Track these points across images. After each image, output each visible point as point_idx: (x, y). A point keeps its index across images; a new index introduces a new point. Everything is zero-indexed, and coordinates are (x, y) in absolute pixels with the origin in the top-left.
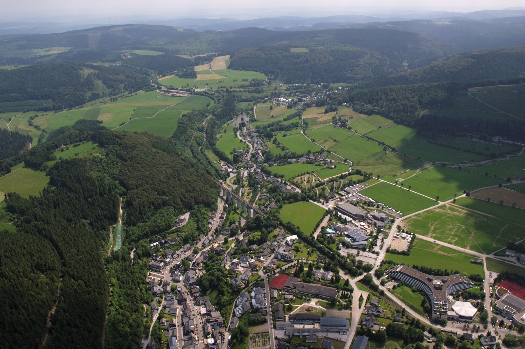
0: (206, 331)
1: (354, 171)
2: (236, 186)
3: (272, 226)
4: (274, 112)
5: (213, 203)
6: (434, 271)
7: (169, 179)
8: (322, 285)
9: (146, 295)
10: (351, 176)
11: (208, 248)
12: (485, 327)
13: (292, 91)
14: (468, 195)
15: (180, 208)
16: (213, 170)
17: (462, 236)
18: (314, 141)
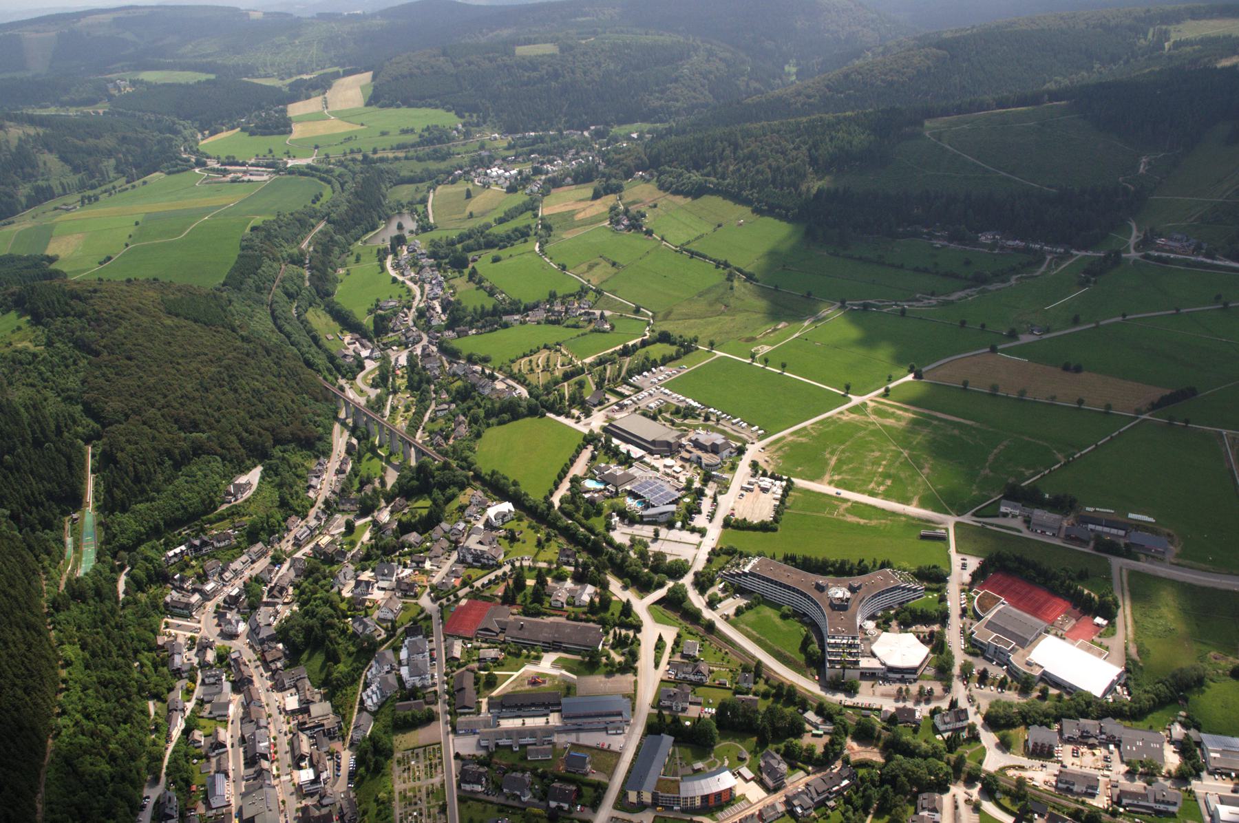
0: (297, 753)
1: (656, 334)
2: (379, 391)
3: (455, 484)
4: (474, 205)
5: (320, 439)
6: (833, 565)
7: (207, 390)
8: (568, 618)
9: (154, 678)
10: (648, 348)
11: (307, 549)
12: (947, 689)
13: (520, 150)
14: (918, 376)
15: (237, 457)
16: (323, 356)
17: (902, 475)
18: (564, 268)
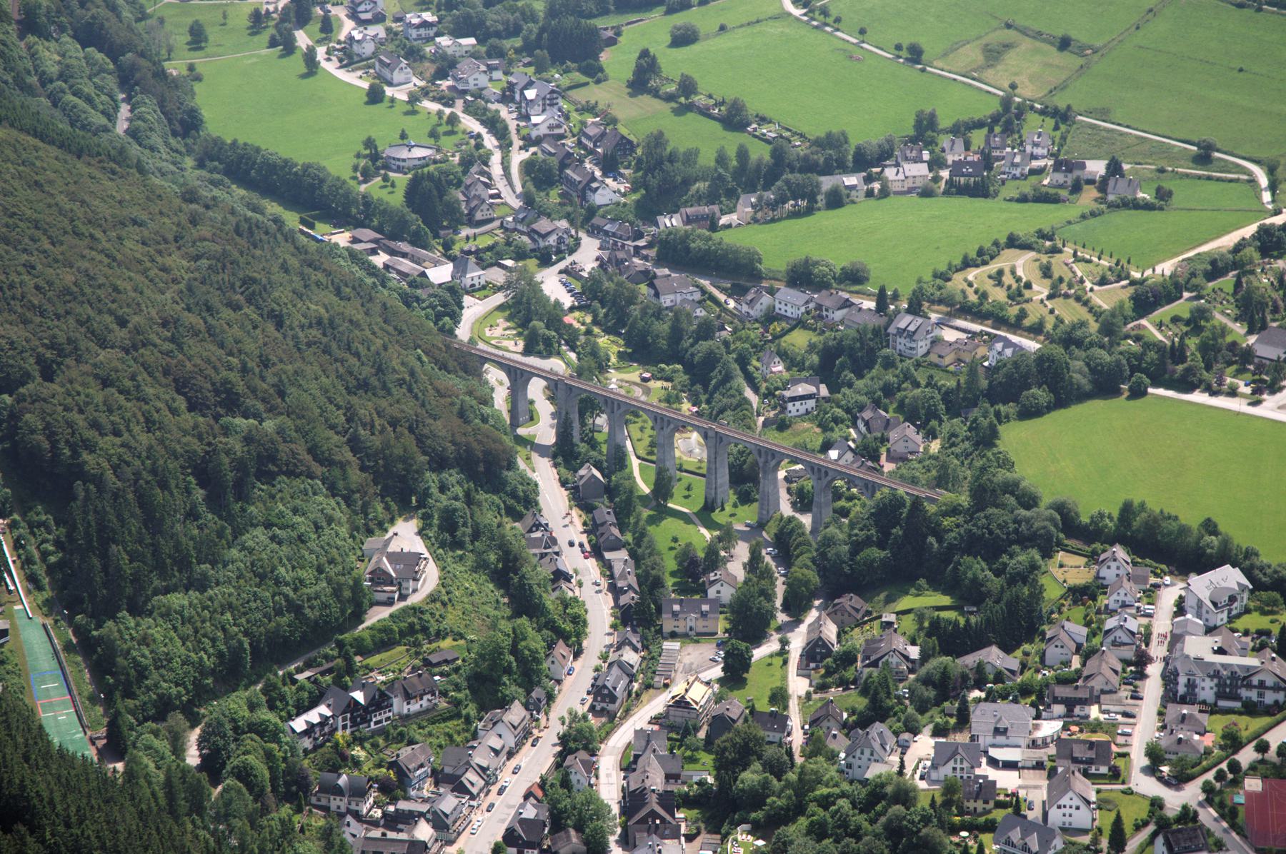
3: (1027, 540)
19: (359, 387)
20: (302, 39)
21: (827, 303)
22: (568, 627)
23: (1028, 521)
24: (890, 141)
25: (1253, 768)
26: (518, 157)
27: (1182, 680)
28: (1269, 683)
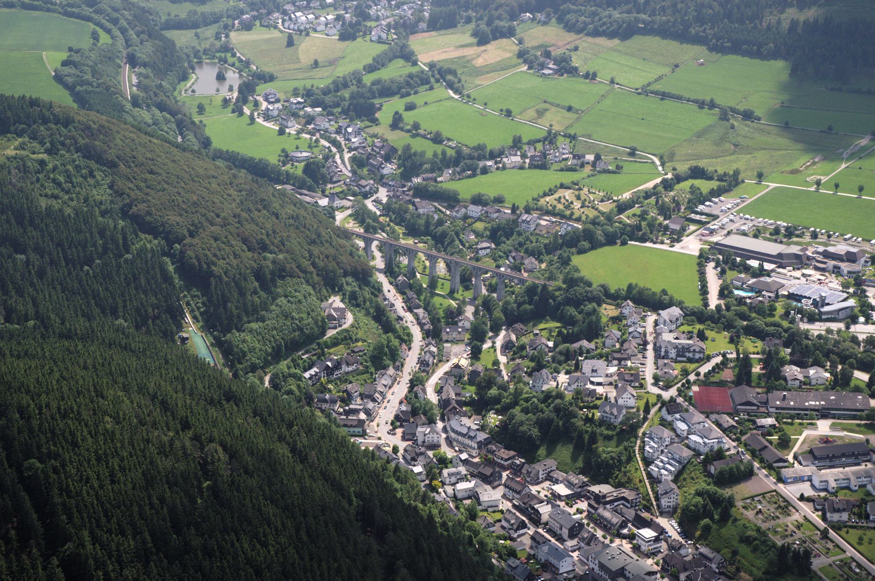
3: (591, 299)
19: (312, 243)
20: (247, 111)
21: (490, 211)
22: (406, 338)
23: (591, 292)
24: (503, 147)
25: (695, 382)
26: (347, 156)
27: (663, 350)
28: (697, 350)
